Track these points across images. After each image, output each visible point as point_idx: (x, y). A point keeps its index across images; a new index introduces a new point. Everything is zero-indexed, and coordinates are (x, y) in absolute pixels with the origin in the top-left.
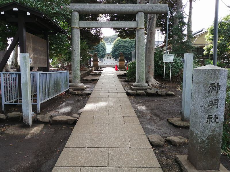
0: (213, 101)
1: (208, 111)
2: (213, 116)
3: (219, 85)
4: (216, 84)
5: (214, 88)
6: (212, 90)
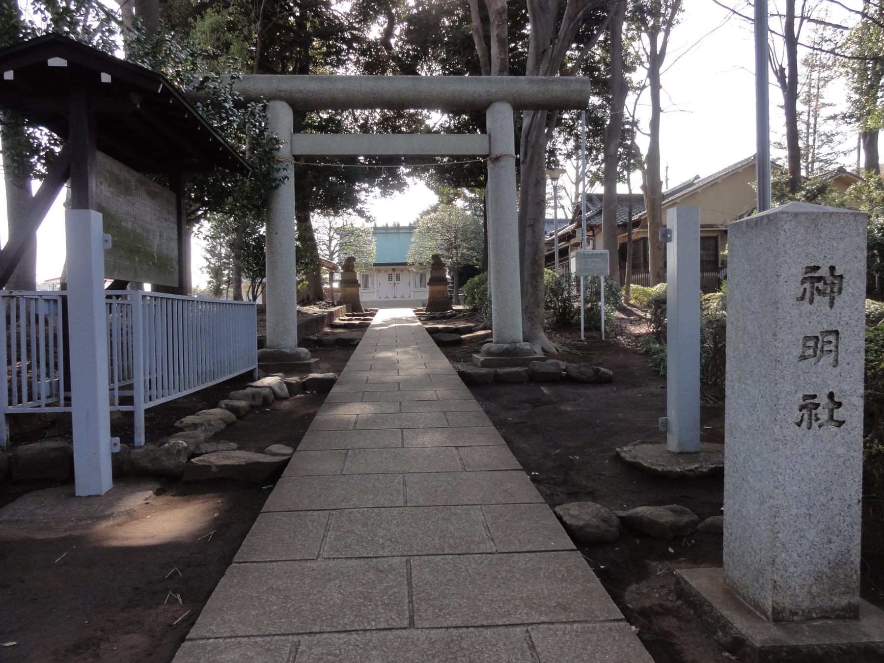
0: (817, 338)
1: (802, 378)
2: (823, 400)
3: (838, 272)
4: (824, 272)
5: (820, 285)
6: (812, 294)
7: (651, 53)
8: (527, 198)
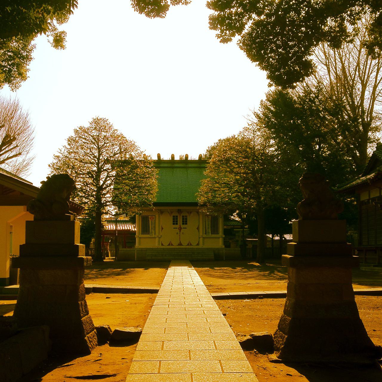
7: (330, 72)
8: (181, 167)
